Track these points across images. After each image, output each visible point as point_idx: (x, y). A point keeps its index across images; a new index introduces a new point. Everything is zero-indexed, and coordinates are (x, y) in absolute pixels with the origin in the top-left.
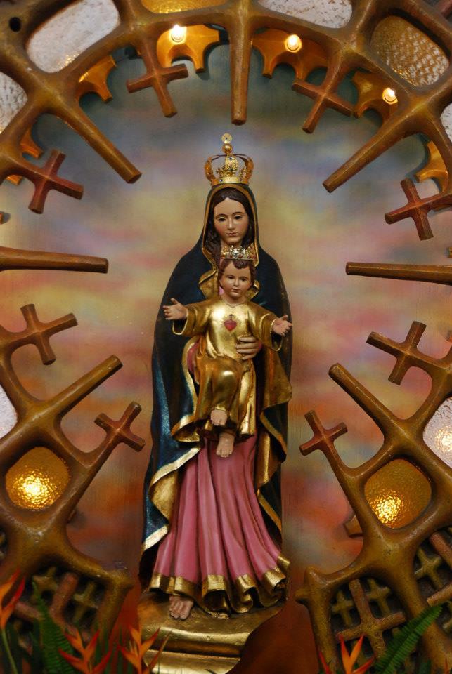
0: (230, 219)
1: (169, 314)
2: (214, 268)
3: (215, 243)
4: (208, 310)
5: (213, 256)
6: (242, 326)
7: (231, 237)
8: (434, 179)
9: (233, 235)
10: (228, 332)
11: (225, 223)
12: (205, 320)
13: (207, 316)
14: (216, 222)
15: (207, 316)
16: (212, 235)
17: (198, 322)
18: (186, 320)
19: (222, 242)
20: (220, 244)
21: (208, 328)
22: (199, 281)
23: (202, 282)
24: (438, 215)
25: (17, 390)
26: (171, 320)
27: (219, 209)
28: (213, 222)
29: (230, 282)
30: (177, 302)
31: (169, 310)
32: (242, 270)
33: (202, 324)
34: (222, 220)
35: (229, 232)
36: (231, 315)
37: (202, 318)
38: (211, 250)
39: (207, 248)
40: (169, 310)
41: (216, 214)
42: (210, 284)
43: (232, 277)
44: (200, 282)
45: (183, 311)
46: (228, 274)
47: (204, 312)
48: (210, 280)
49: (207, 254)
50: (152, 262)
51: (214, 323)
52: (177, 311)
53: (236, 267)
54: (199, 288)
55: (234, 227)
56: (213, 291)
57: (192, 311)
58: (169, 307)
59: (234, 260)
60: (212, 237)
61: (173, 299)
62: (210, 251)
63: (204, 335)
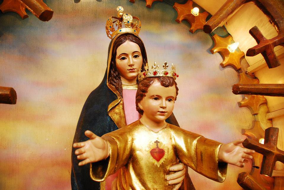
0: (130, 56)
1: (84, 155)
2: (119, 97)
3: (118, 79)
4: (130, 139)
5: (117, 89)
6: (169, 154)
7: (131, 72)
8: (219, 52)
9: (132, 71)
10: (156, 162)
11: (126, 61)
12: (127, 152)
13: (129, 146)
14: (118, 61)
15: (129, 146)
16: (114, 73)
17: (122, 152)
18: (109, 157)
19: (122, 79)
20: (121, 80)
21: (131, 158)
22: (107, 110)
23: (111, 109)
24: (225, 70)
25: (239, 9)
26: (88, 164)
27: (120, 50)
28: (115, 62)
29: (155, 104)
30: (94, 135)
31: (82, 150)
32: (170, 88)
33: (125, 157)
34: (124, 59)
35: (130, 68)
36: (157, 142)
37: (125, 149)
38: (115, 84)
39: (111, 83)
40: (82, 150)
41: (118, 54)
42: (117, 110)
43: (157, 98)
44: (108, 111)
45: (104, 148)
46: (152, 94)
47: (126, 142)
48: (117, 107)
49: (111, 87)
50: (70, 100)
51: (138, 153)
52: (96, 150)
53: (163, 85)
54: (108, 115)
55: (134, 63)
56: (121, 117)
57: (112, 142)
58: (82, 144)
59: (159, 78)
60: (115, 75)
61: (88, 132)
62: (113, 85)
63: (126, 166)
